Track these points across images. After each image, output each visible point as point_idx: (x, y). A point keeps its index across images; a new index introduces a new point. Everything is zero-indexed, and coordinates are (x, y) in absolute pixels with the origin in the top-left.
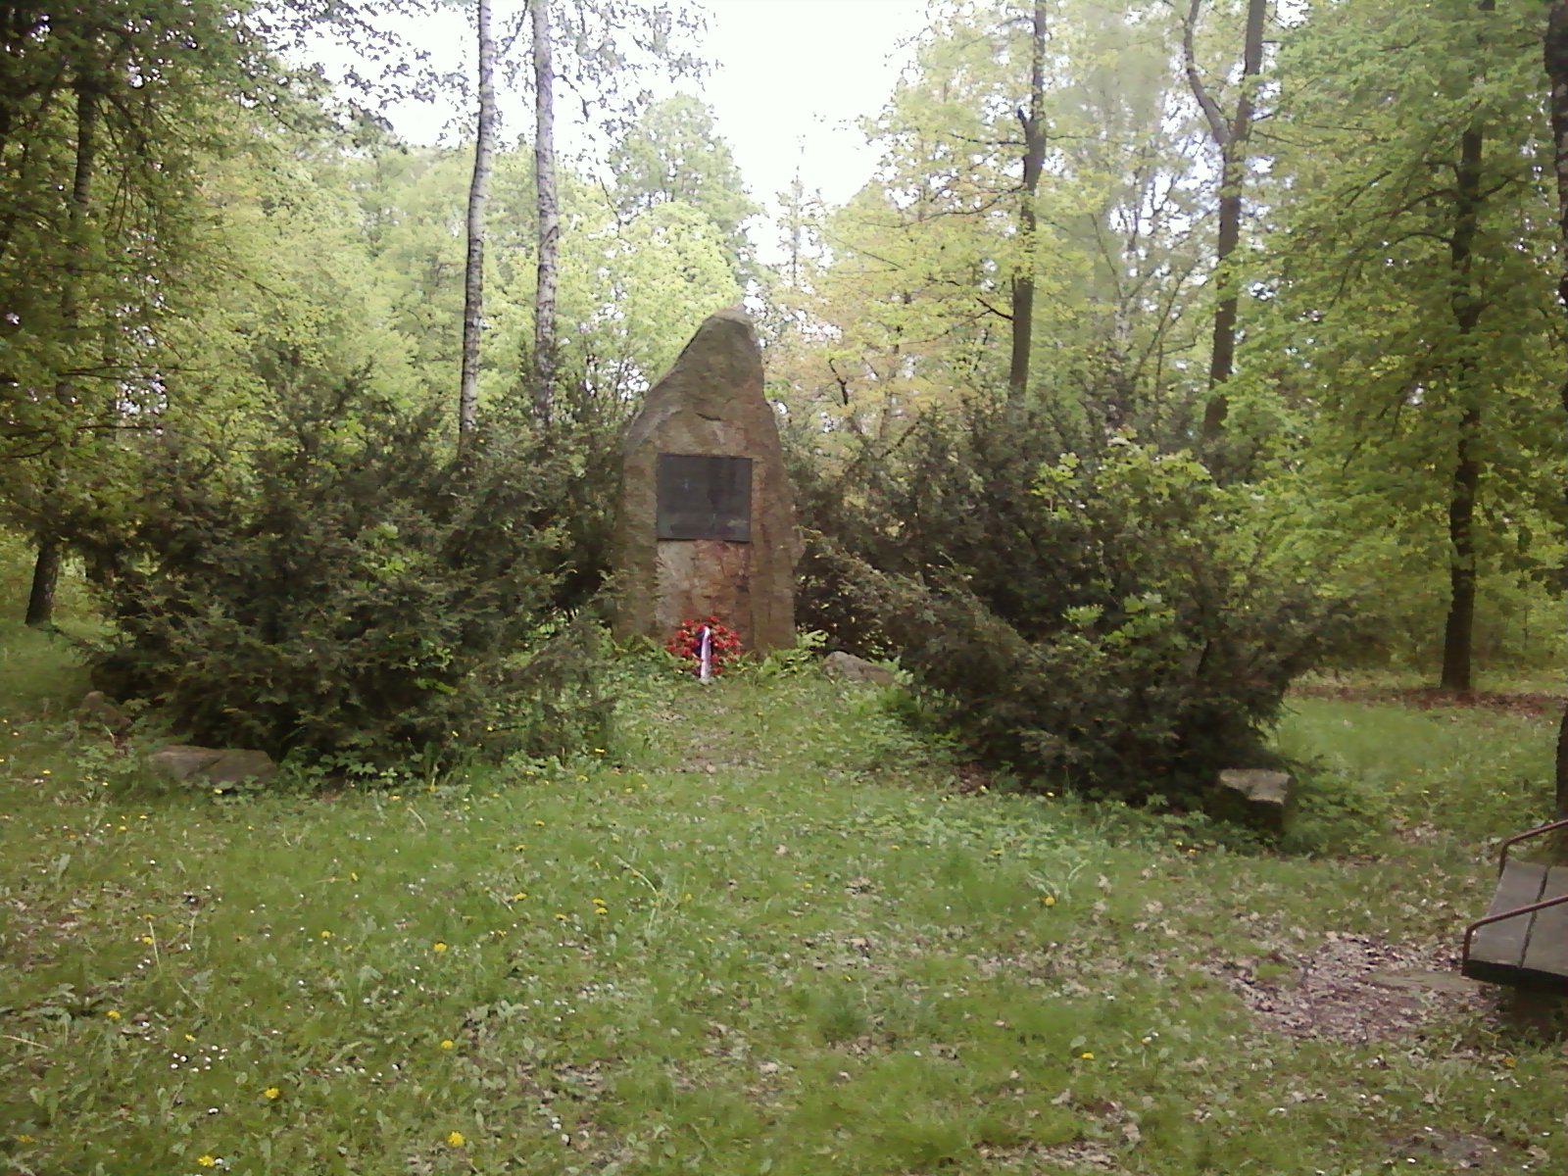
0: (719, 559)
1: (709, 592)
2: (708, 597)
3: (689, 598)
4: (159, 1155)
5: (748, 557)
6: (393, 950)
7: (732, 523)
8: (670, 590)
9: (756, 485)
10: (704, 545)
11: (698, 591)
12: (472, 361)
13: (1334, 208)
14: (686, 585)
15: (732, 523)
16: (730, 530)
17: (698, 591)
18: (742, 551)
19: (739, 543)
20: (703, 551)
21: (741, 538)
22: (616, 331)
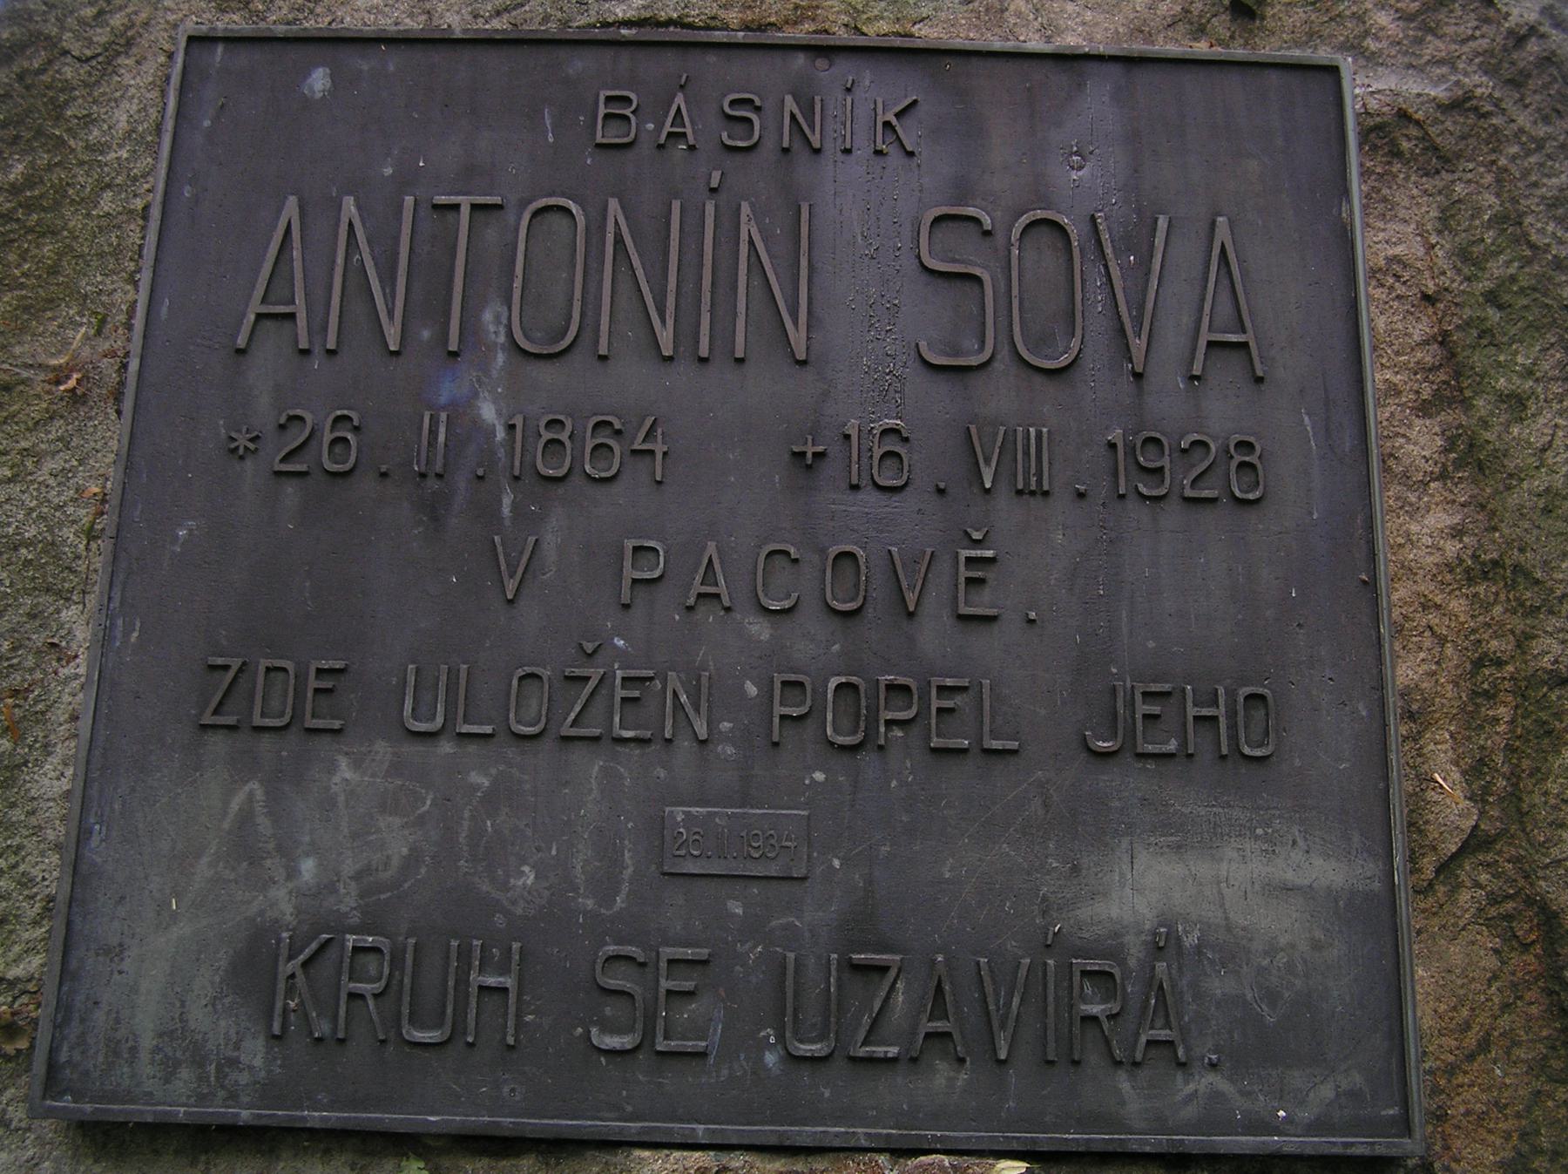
4: (1478, 360)
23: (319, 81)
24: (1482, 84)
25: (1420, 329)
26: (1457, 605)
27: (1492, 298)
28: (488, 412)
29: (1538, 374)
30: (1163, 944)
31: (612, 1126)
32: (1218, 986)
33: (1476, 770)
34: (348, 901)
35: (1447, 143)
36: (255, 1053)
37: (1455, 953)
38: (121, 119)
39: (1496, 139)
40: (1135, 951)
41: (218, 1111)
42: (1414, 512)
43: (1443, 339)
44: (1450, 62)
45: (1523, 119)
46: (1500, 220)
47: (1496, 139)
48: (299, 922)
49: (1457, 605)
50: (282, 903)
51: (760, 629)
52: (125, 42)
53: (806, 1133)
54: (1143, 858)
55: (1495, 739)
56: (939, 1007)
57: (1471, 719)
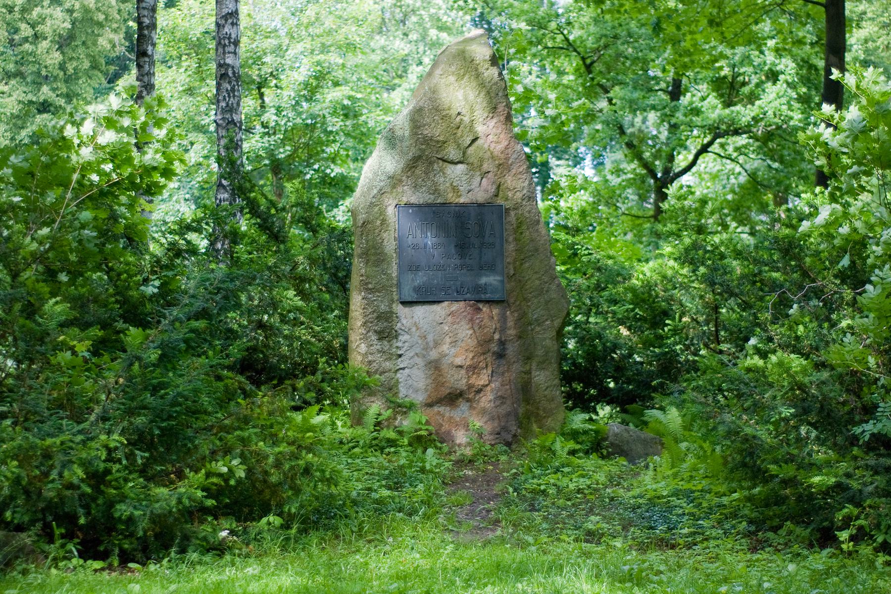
5: (503, 319)
7: (484, 280)
15: (484, 280)
17: (446, 361)
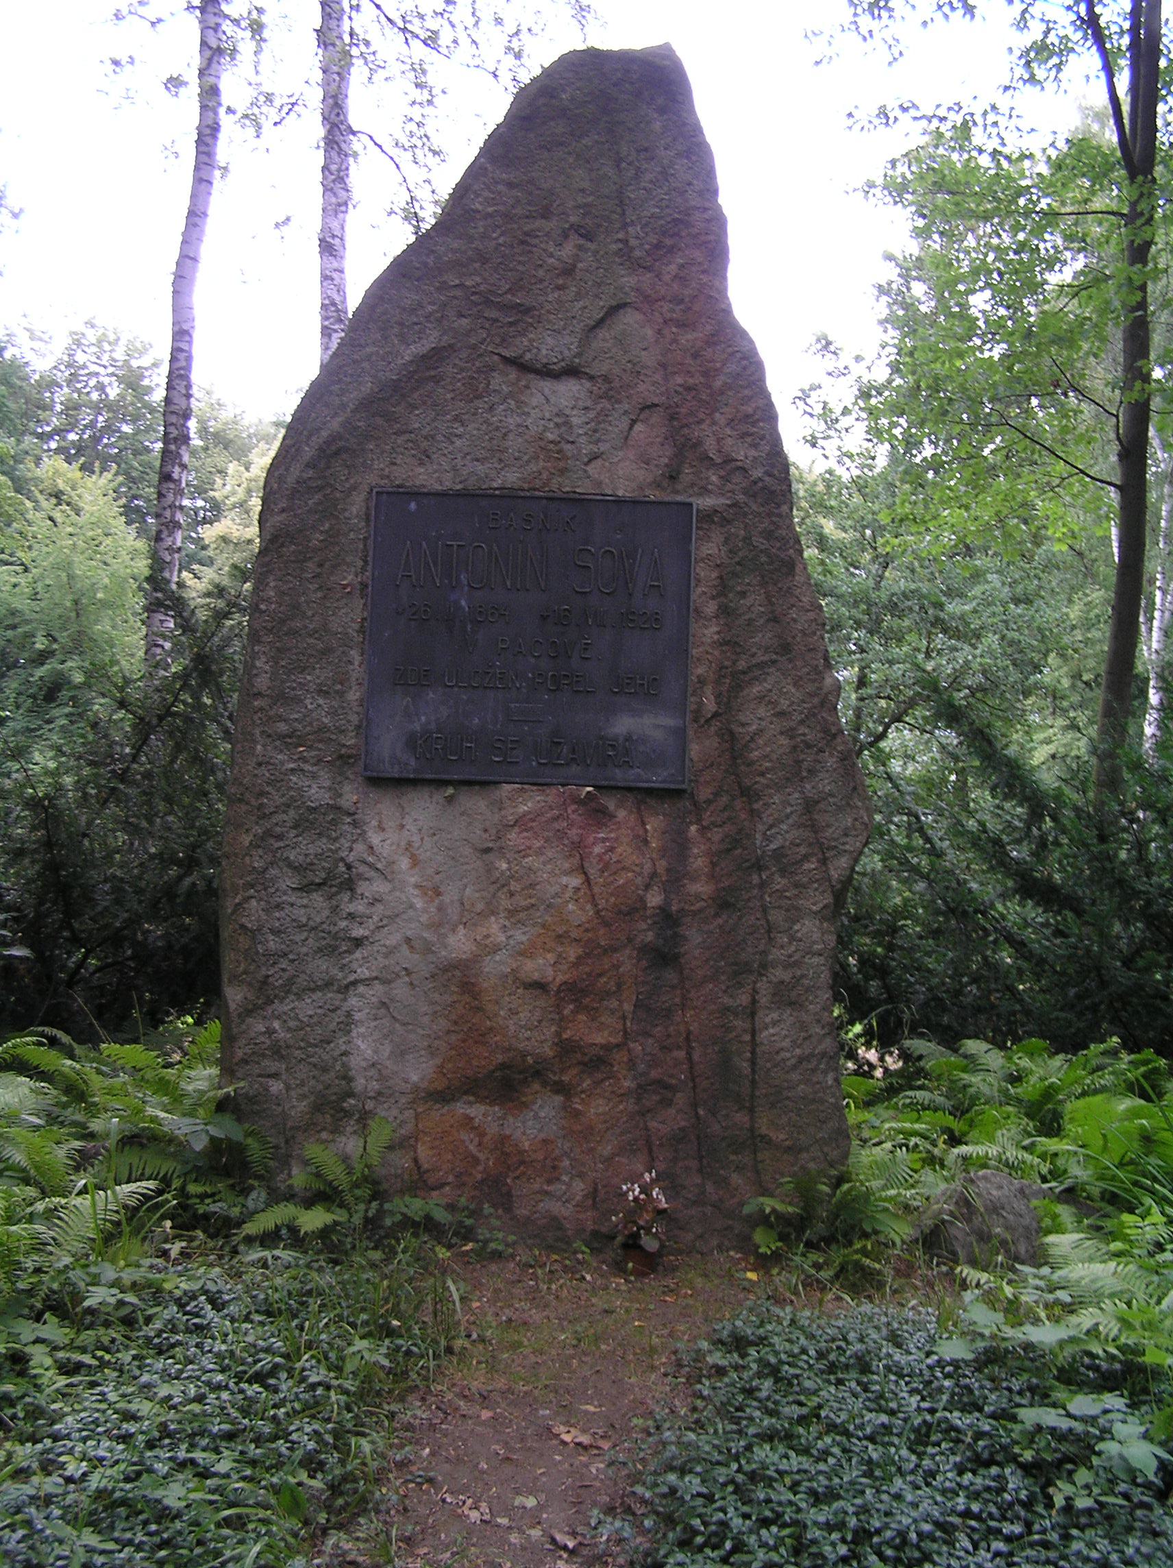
0: (579, 848)
1: (539, 967)
2: (540, 986)
3: (469, 988)
4: (731, 583)
5: (678, 847)
6: (664, 1444)
8: (406, 957)
9: (702, 596)
10: (529, 802)
11: (495, 967)
12: (169, 541)
13: (762, 1341)
14: (459, 944)
15: (623, 725)
16: (623, 750)
17: (495, 967)
18: (654, 824)
19: (646, 795)
20: (521, 823)
21: (656, 779)
22: (430, 261)
23: (413, 506)
24: (741, 497)
25: (714, 575)
26: (716, 653)
27: (739, 563)
28: (463, 603)
29: (291, 957)
30: (628, 738)
31: (497, 779)
32: (641, 748)
33: (718, 696)
34: (433, 726)
35: (729, 517)
36: (413, 762)
37: (707, 743)
38: (354, 511)
39: (745, 515)
40: (621, 740)
41: (405, 775)
42: (706, 627)
43: (721, 577)
44: (732, 491)
45: (754, 507)
46: (744, 539)
47: (745, 515)
48: (862, 699)
49: (716, 653)
50: (417, 727)
51: (533, 660)
52: (354, 488)
53: (540, 781)
54: (742, 718)
55: (724, 688)
56: (574, 752)
57: (717, 682)
